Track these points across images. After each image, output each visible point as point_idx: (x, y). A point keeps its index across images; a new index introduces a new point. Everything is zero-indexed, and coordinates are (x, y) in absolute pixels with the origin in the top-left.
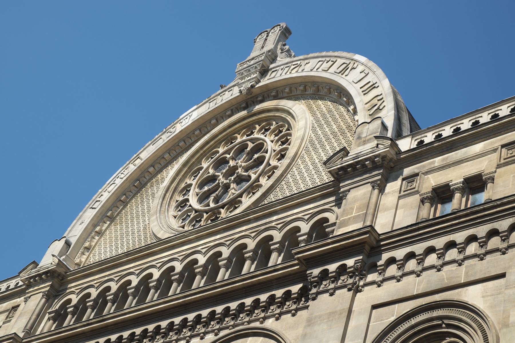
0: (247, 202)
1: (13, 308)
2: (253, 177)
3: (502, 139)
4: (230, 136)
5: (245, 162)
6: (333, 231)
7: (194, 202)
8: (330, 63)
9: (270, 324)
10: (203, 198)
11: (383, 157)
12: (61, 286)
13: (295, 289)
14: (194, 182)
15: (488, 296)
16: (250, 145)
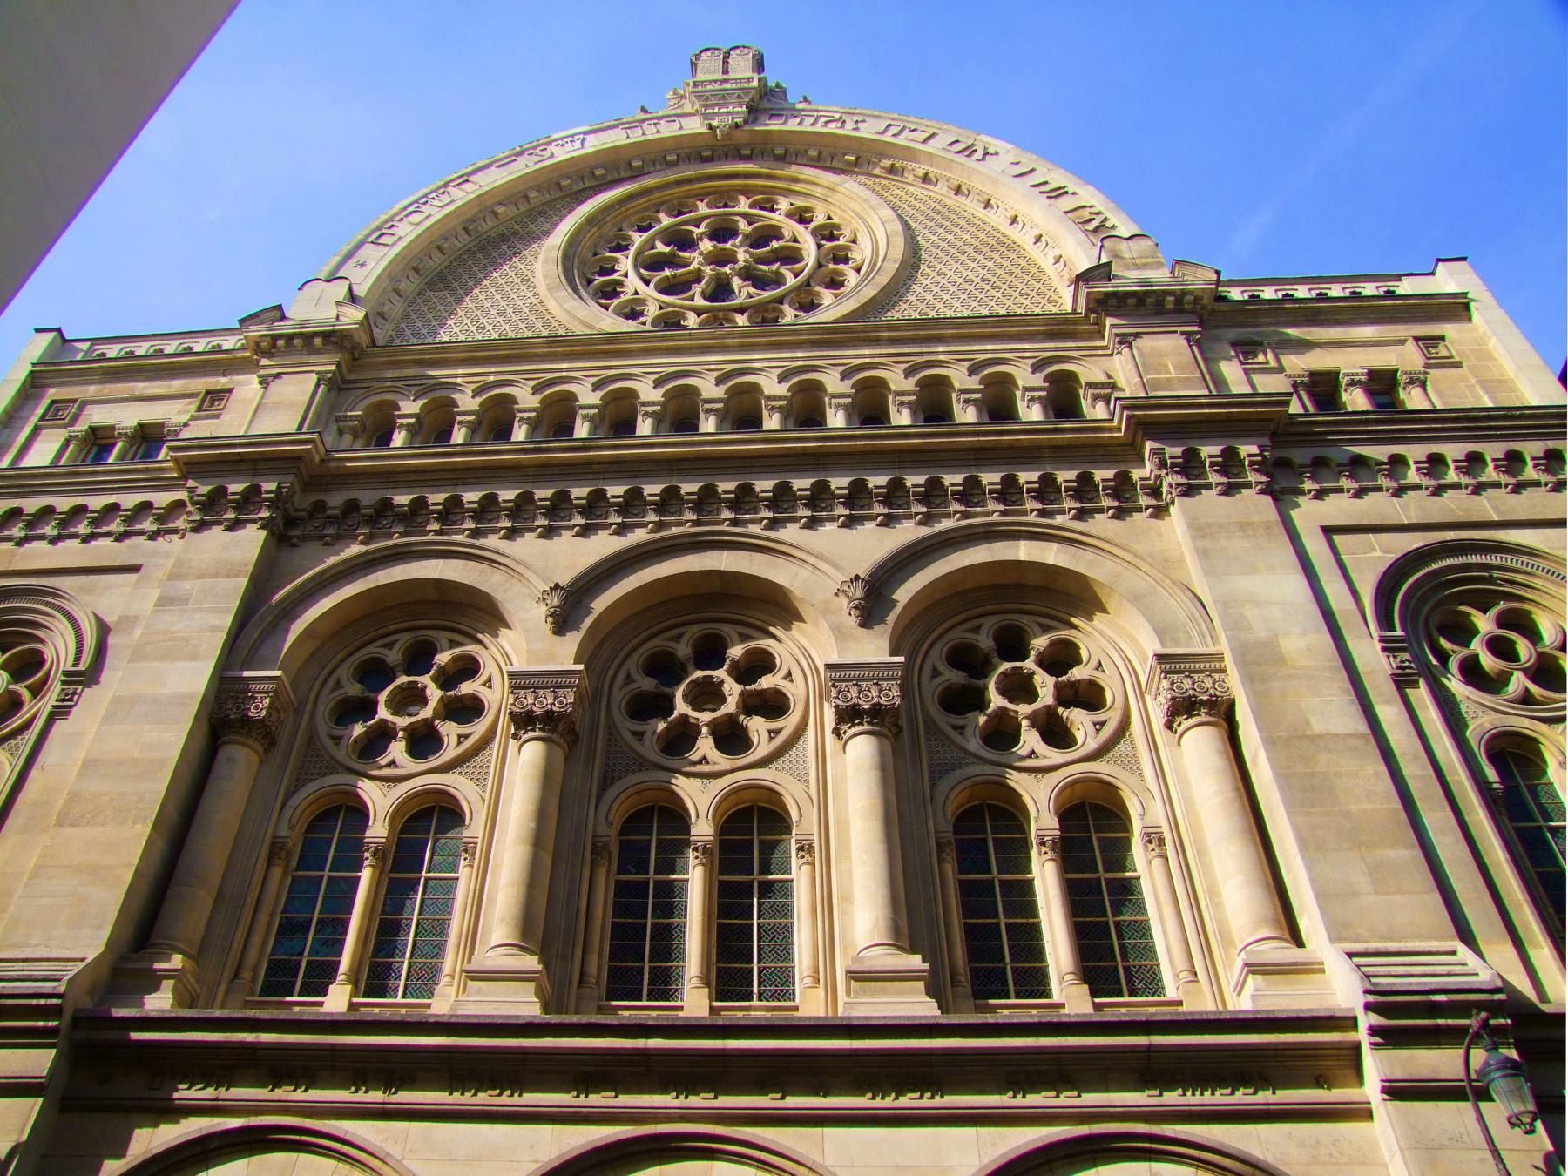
4: (677, 198)
12: (350, 371)
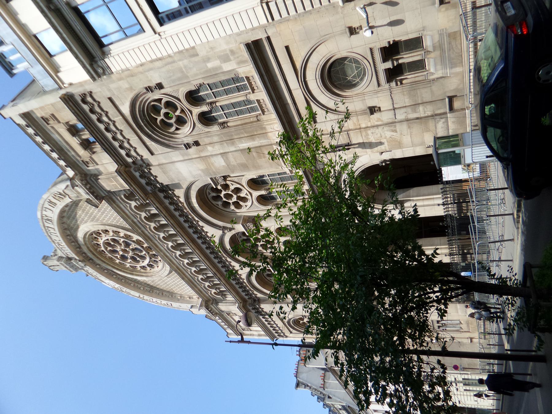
0: (135, 237)
2: (122, 240)
5: (117, 247)
6: (129, 190)
7: (147, 261)
8: (49, 229)
9: (182, 199)
10: (143, 258)
11: (82, 180)
12: (210, 300)
13: (161, 195)
14: (138, 266)
16: (109, 248)
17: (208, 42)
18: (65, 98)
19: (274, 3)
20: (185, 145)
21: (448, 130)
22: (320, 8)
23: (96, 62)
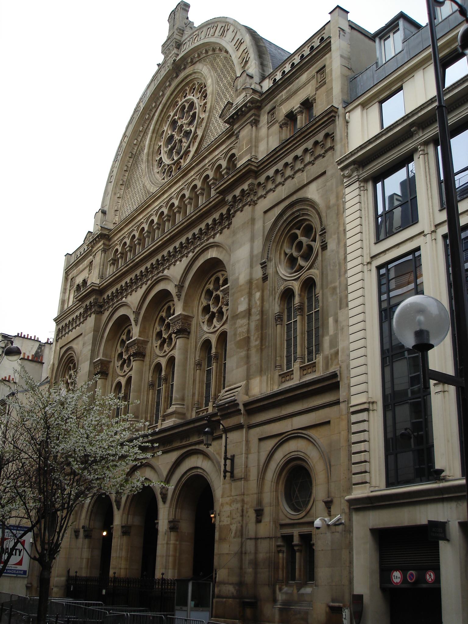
1: (90, 263)
3: (316, 67)
8: (215, 28)
15: (319, 189)
17: (349, 326)
18: (332, 111)
19: (366, 419)
20: (265, 262)
21: (226, 598)
22: (351, 471)
23: (357, 169)
